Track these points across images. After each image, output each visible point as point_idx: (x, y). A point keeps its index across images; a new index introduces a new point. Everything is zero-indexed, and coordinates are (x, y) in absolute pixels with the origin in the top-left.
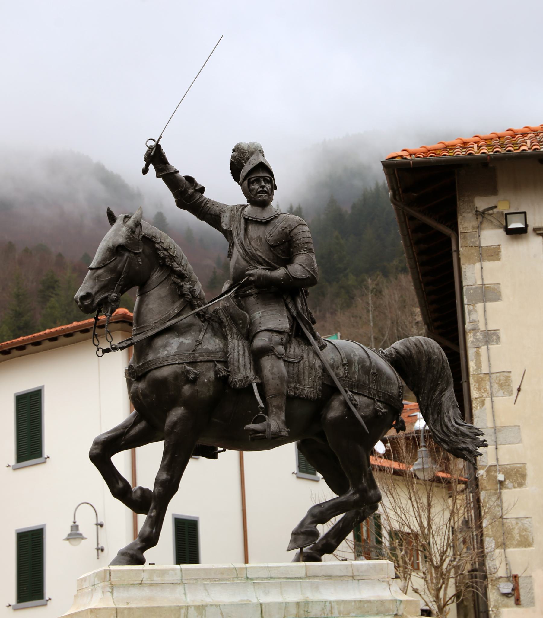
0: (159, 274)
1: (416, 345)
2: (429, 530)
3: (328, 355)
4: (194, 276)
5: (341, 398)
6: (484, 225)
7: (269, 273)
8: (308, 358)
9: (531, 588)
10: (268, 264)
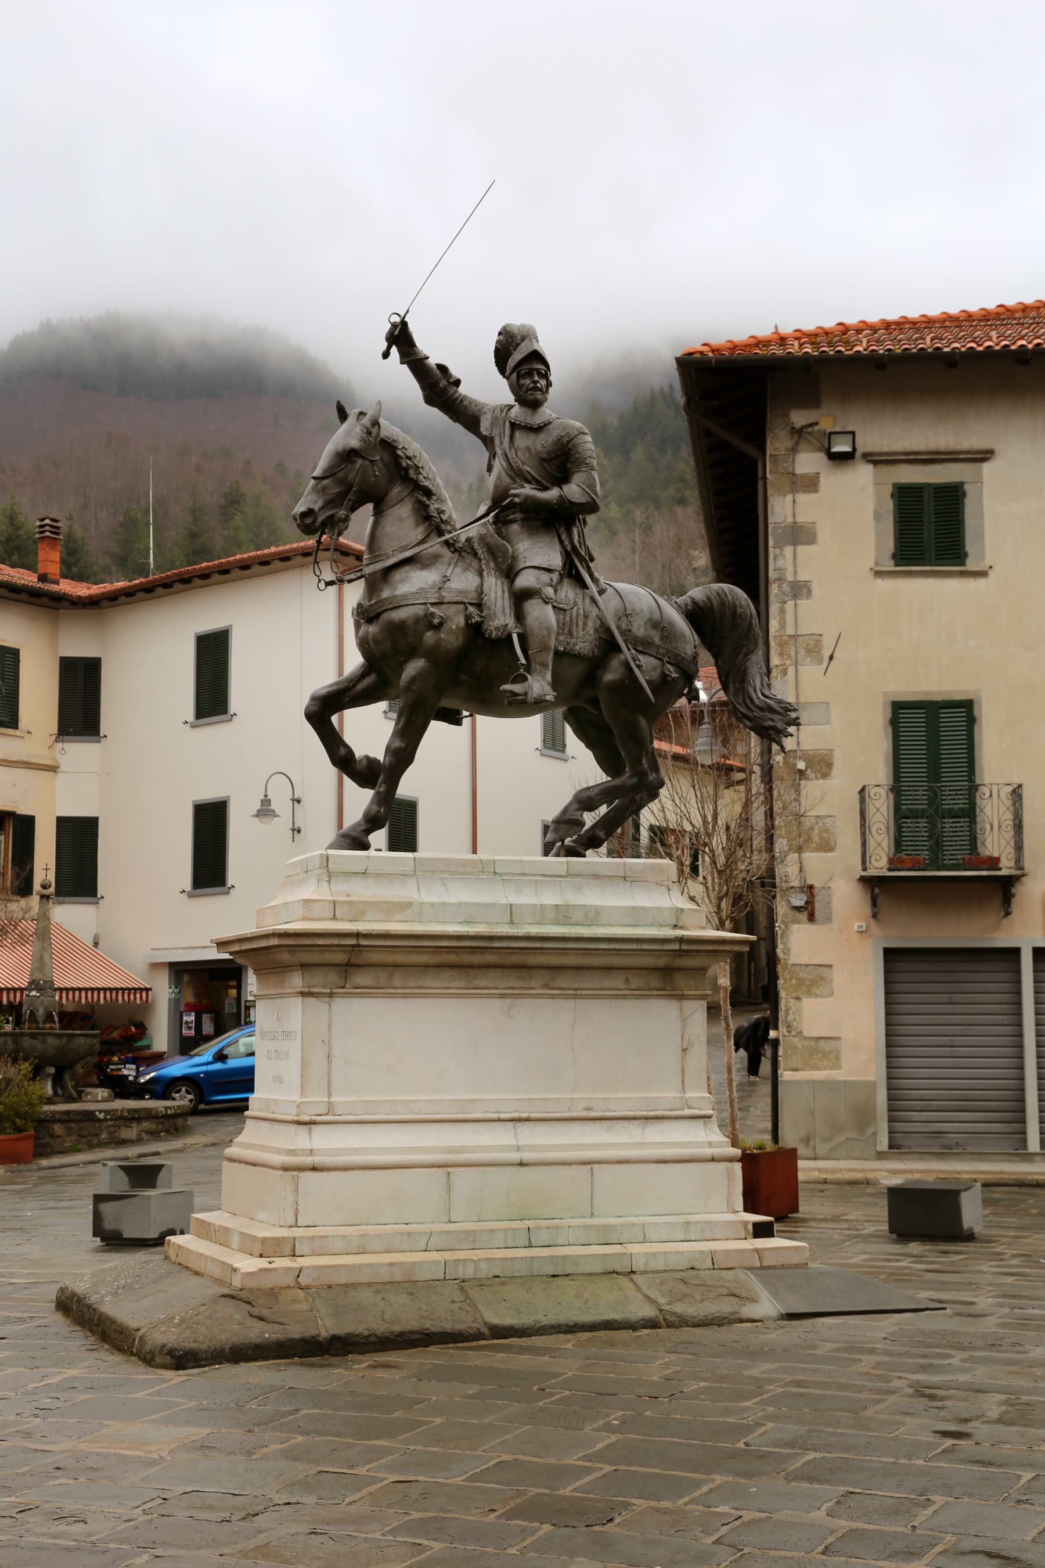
0: (399, 489)
1: (718, 594)
2: (714, 827)
3: (609, 605)
4: (445, 493)
5: (622, 657)
6: (800, 447)
7: (539, 494)
8: (584, 604)
9: (829, 902)
10: (538, 483)
